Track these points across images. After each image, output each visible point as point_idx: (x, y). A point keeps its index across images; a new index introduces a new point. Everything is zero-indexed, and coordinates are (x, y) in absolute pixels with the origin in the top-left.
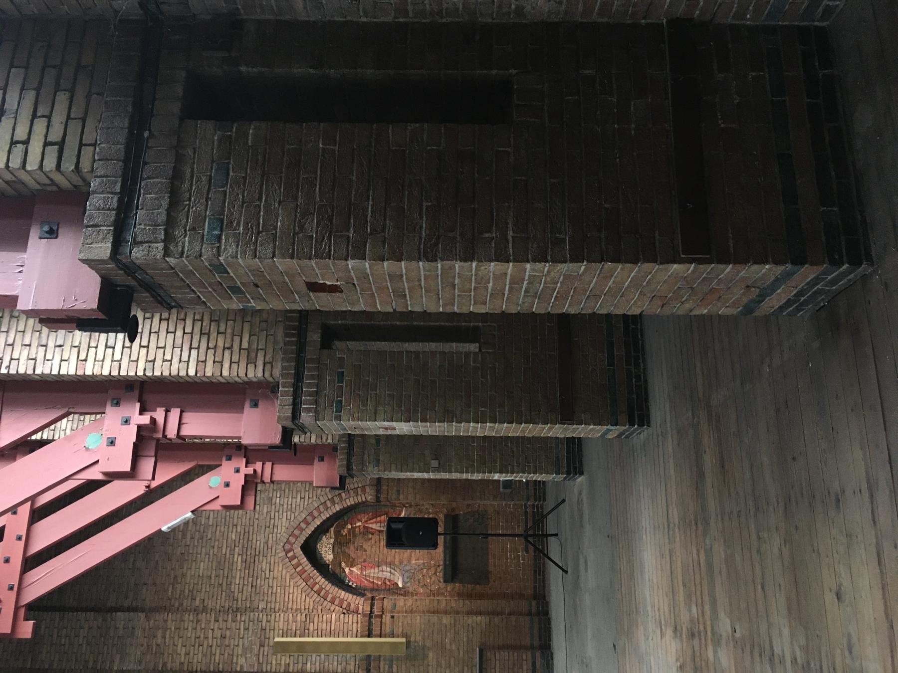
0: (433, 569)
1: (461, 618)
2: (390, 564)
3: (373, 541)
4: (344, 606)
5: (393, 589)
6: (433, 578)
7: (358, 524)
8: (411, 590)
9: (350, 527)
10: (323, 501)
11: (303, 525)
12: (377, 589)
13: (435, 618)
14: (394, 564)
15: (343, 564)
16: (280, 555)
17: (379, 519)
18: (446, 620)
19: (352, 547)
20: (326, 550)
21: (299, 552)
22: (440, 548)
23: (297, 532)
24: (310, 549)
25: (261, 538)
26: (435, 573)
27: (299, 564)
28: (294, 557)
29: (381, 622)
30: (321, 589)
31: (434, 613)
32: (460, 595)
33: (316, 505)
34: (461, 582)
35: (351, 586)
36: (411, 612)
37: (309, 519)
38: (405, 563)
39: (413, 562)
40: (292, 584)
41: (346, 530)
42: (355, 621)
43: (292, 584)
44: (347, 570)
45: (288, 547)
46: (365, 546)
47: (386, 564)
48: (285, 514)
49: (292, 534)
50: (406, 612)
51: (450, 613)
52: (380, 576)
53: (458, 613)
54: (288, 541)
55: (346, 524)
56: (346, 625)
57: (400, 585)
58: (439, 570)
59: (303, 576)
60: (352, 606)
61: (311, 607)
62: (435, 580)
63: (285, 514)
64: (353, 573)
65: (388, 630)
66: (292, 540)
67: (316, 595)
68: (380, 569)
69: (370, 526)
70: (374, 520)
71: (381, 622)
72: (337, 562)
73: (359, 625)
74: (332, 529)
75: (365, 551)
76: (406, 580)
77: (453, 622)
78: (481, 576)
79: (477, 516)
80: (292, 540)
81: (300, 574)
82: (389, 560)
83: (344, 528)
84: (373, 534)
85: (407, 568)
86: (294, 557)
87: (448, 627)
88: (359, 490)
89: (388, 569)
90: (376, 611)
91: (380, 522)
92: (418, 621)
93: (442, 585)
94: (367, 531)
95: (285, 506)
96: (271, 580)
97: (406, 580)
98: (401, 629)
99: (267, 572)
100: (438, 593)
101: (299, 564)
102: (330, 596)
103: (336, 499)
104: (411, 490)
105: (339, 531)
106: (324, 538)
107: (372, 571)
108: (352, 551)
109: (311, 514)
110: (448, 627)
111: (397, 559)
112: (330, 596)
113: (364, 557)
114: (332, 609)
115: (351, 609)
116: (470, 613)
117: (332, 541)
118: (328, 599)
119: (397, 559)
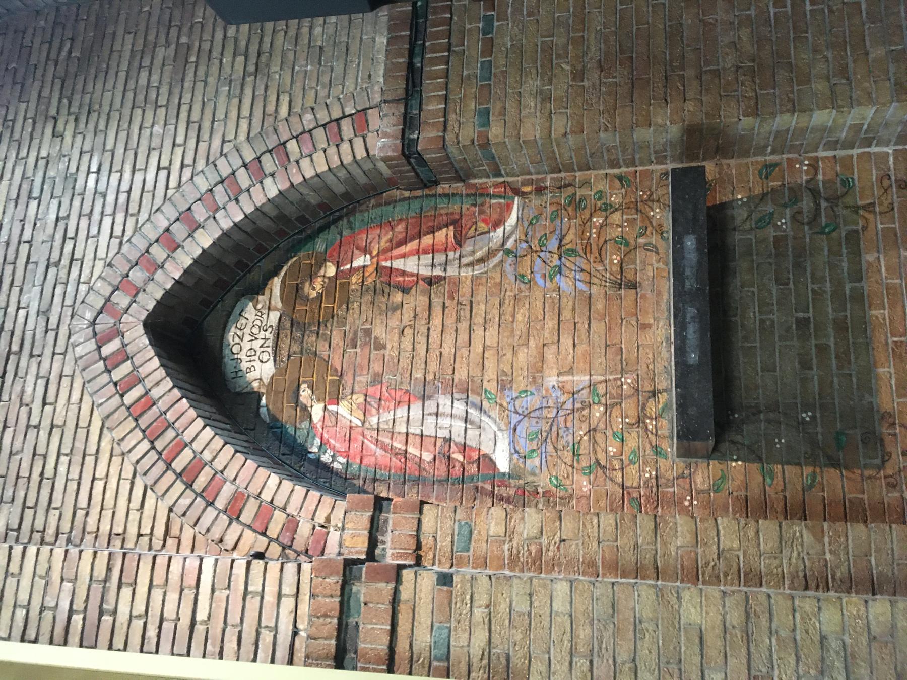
0: (630, 407)
1: (780, 604)
2: (466, 390)
3: (408, 315)
4: (273, 531)
5: (469, 478)
6: (632, 442)
7: (359, 262)
8: (544, 481)
9: (331, 270)
10: (225, 171)
11: (159, 254)
12: (411, 477)
13: (642, 598)
14: (480, 390)
15: (305, 394)
16: (79, 350)
17: (427, 240)
18: (698, 608)
19: (336, 338)
20: (253, 348)
21: (138, 338)
22: (704, 164)
23: (137, 276)
24: (188, 335)
25: (31, 298)
26: (640, 420)
27: (135, 380)
28: (123, 356)
29: (395, 601)
30: (196, 466)
31: (638, 572)
32: (752, 508)
33: (203, 184)
34: (753, 454)
35: (327, 468)
36: (537, 562)
37: (179, 231)
38: (521, 383)
39: (552, 380)
40: (106, 445)
41: (318, 284)
42: (288, 589)
43: (106, 445)
44: (317, 411)
45: (106, 322)
46: (379, 331)
47: (450, 388)
48: (107, 221)
49: (123, 284)
50: (514, 561)
51: (716, 580)
52: (429, 430)
53: (754, 578)
54: (107, 306)
55: (321, 264)
56: (253, 604)
57: (503, 465)
58: (652, 408)
59: (144, 422)
60: (304, 529)
61: (160, 531)
62: (646, 445)
63: (107, 221)
64: (334, 424)
65: (423, 639)
66: (122, 300)
67: (179, 486)
68: (431, 406)
69: (398, 264)
70: (413, 245)
71: (395, 601)
72: (287, 385)
73: (304, 608)
74: (277, 282)
75: (380, 346)
76: (524, 445)
77: (735, 617)
78: (844, 434)
79: (806, 204)
80: (122, 300)
81: (136, 412)
82: (461, 375)
83: (311, 277)
84: (405, 290)
85: (533, 401)
86: (123, 356)
87: (714, 641)
88: (346, 125)
89: (459, 407)
90: (392, 551)
91: (433, 250)
92: (560, 605)
93: (671, 464)
94: (389, 281)
95: (111, 198)
96: (43, 434)
97: (524, 445)
98: (480, 638)
99: (36, 407)
100: (655, 500)
101: (135, 380)
102: (227, 490)
103: (268, 164)
104: (531, 102)
105: (298, 288)
106: (250, 312)
107: (401, 412)
108: (333, 347)
109: (185, 216)
110: (714, 641)
111: (491, 373)
112: (227, 490)
113: (377, 367)
114: (230, 540)
115: (299, 545)
116: (815, 581)
117: (274, 317)
118: (220, 503)
119: (491, 373)
